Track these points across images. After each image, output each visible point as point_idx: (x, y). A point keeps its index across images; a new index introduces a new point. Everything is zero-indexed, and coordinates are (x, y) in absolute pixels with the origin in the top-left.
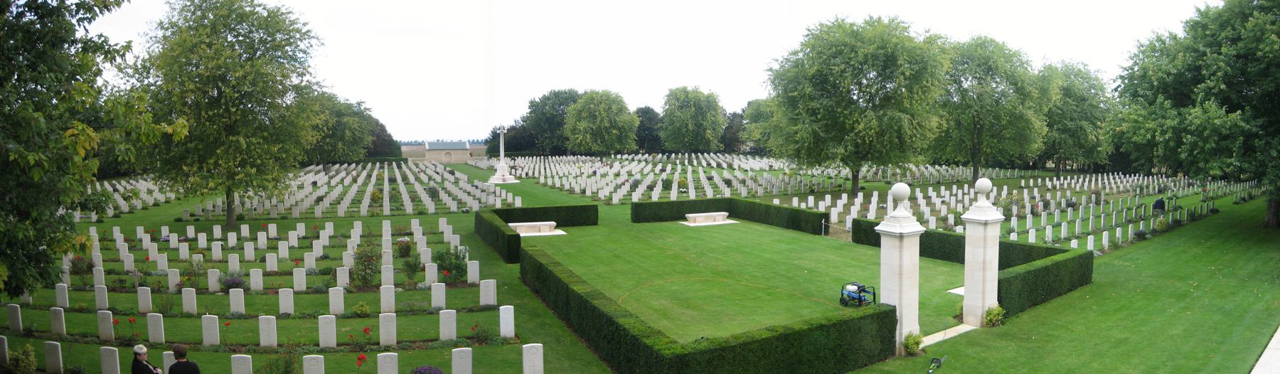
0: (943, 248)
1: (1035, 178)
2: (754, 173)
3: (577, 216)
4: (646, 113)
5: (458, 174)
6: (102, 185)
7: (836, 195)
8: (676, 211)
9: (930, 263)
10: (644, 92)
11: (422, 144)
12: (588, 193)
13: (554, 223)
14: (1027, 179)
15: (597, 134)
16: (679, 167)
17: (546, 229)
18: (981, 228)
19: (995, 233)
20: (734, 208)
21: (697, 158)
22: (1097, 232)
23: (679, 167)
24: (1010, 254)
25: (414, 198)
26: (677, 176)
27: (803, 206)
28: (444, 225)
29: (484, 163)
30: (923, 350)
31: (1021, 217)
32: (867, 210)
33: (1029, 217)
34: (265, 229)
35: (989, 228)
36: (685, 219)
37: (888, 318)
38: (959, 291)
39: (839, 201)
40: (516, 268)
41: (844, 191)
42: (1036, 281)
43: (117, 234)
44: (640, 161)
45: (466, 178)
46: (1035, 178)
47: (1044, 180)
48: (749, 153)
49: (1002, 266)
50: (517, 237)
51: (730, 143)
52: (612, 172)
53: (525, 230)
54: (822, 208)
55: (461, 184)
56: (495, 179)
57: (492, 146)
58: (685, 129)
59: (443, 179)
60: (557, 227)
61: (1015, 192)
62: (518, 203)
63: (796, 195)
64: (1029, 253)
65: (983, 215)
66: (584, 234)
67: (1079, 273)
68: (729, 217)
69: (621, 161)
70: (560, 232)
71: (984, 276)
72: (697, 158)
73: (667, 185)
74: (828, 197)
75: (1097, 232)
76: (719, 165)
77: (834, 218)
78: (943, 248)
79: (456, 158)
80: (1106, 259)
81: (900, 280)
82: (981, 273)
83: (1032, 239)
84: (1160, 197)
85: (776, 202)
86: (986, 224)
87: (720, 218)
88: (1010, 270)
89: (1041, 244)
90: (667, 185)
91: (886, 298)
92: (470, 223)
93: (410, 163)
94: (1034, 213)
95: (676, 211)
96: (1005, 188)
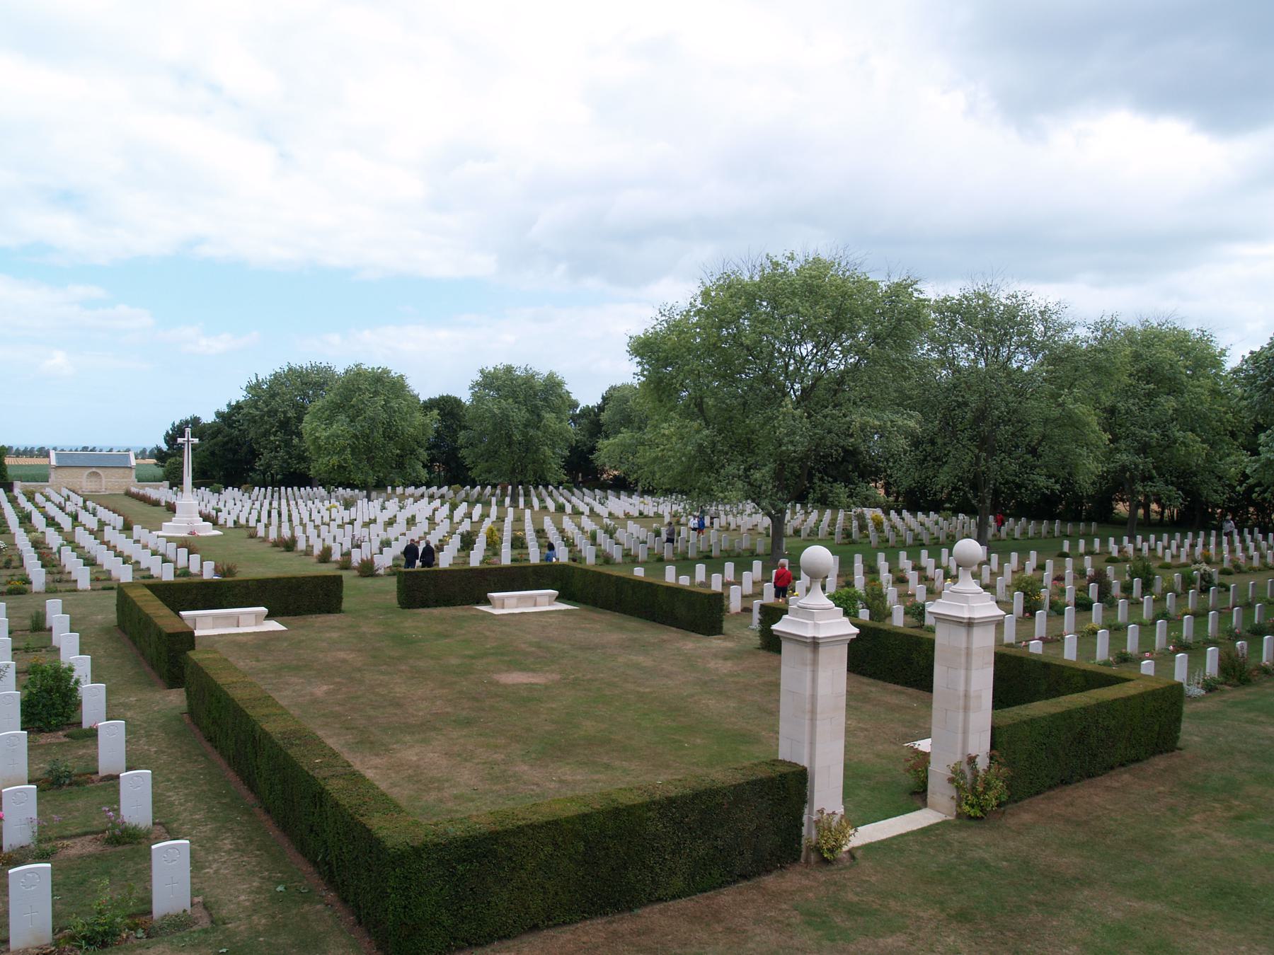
0: (892, 660)
1: (1089, 538)
2: (608, 525)
3: (305, 594)
4: (446, 407)
5: (104, 514)
6: (708, 576)
7: (743, 564)
8: (471, 587)
9: (852, 675)
10: (439, 364)
11: (43, 453)
12: (336, 556)
13: (263, 609)
14: (1073, 539)
15: (364, 448)
16: (494, 510)
17: (251, 621)
18: (962, 631)
19: (984, 642)
20: (573, 583)
21: (527, 494)
22: (1194, 650)
23: (494, 510)
24: (1015, 678)
25: (48, 560)
26: (487, 523)
27: (684, 581)
28: (56, 614)
29: (161, 492)
30: (851, 853)
31: (1057, 610)
32: (497, 553)
33: (1069, 611)
34: (721, 571)
35: (977, 633)
36: (487, 602)
37: (792, 785)
38: (924, 745)
39: (746, 575)
40: (176, 699)
41: (758, 557)
42: (1068, 734)
43: (882, 564)
44: (432, 497)
45: (119, 521)
46: (1089, 538)
47: (1104, 542)
48: (611, 487)
49: (1000, 701)
50: (187, 639)
51: (583, 471)
52: (384, 517)
53: (207, 624)
54: (716, 585)
55: (109, 533)
56: (176, 527)
57: (166, 461)
58: (502, 439)
59: (102, 524)
60: (269, 616)
61: (1049, 563)
62: (209, 573)
63: (700, 560)
64: (1054, 678)
65: (969, 604)
66: (321, 629)
67: (1151, 727)
68: (559, 599)
69: (402, 498)
70: (274, 626)
71: (966, 721)
72: (527, 494)
73: (468, 542)
74: (729, 567)
75: (1194, 650)
76: (560, 509)
77: (735, 604)
78: (892, 660)
79: (112, 482)
80: (1213, 703)
81: (817, 722)
82: (961, 716)
83: (1070, 651)
84: (339, 573)
85: (639, 572)
86: (970, 624)
87: (543, 601)
88: (1015, 709)
89: (1089, 666)
90: (468, 542)
91: (789, 750)
92: (107, 613)
93: (17, 491)
94: (1083, 606)
95: (471, 587)
96: (1033, 554)
